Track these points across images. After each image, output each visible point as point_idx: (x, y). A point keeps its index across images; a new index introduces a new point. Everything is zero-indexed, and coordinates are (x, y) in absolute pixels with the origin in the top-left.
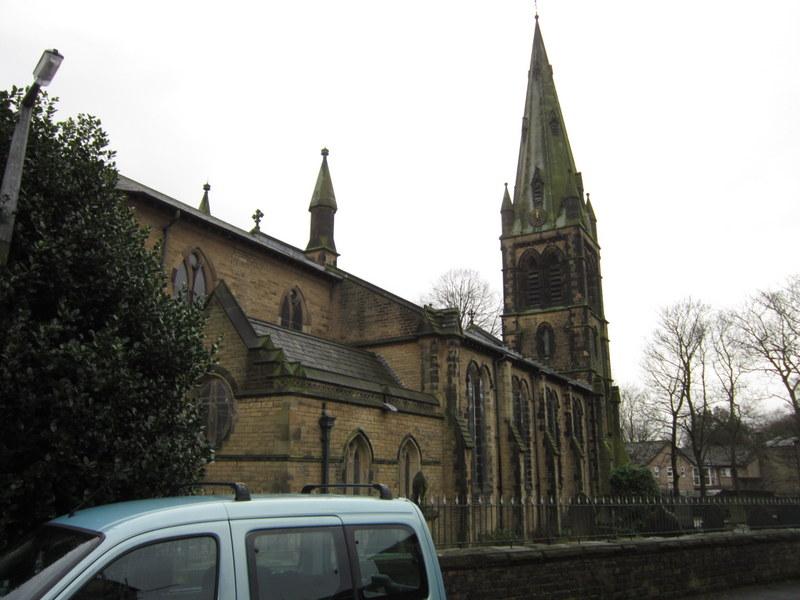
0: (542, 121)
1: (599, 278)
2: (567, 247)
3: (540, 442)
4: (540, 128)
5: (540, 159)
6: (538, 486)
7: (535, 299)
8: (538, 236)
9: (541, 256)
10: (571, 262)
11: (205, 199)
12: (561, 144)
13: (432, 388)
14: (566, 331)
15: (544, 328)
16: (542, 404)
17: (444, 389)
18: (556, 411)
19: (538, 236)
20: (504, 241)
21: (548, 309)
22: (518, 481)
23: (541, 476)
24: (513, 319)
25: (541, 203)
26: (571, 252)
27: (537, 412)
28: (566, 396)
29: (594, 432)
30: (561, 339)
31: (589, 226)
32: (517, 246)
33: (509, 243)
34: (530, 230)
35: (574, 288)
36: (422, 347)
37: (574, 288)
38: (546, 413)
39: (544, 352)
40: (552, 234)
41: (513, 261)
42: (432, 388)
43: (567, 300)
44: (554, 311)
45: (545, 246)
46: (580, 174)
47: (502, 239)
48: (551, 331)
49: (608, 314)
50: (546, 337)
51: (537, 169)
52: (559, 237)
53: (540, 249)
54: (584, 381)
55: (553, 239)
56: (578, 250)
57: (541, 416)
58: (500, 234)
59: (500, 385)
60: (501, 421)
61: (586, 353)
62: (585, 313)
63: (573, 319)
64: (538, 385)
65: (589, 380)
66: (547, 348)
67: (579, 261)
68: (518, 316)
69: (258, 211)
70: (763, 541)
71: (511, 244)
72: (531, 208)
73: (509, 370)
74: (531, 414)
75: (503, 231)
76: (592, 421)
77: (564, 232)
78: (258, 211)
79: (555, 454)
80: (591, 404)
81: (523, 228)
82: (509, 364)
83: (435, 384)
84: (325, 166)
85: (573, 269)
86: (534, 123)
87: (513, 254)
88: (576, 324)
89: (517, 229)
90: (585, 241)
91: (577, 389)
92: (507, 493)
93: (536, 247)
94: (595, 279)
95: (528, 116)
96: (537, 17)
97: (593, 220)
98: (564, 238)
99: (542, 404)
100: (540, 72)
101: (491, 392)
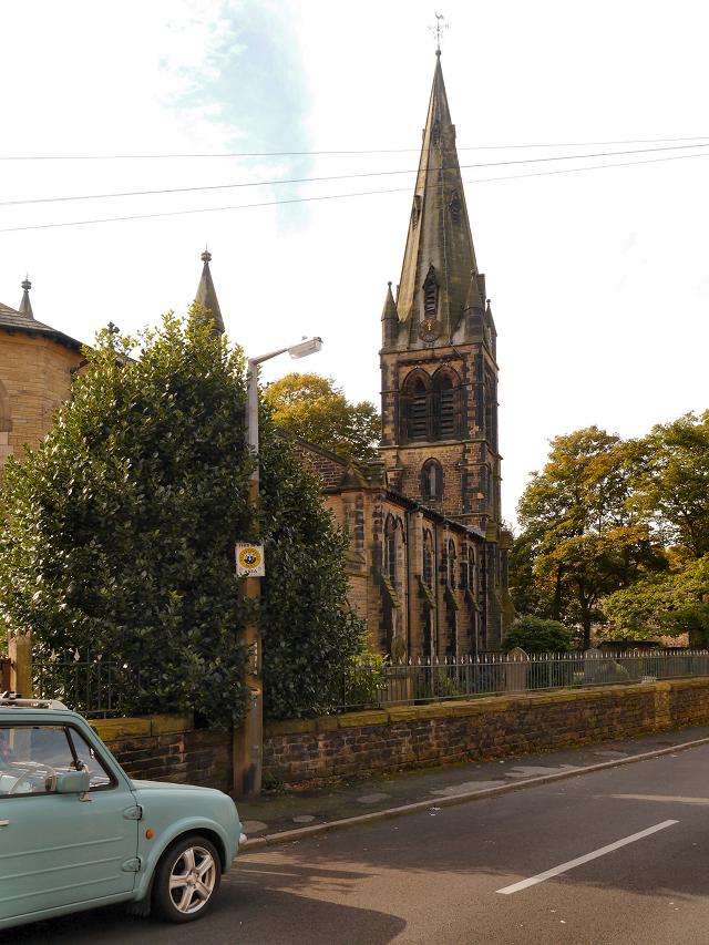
0: (440, 204)
1: (496, 405)
2: (465, 369)
3: (441, 596)
4: (437, 212)
5: (436, 253)
6: (437, 642)
7: (421, 430)
8: (429, 352)
9: (431, 378)
10: (469, 388)
11: (26, 301)
12: (462, 236)
13: (358, 546)
14: (457, 468)
15: (429, 465)
16: (444, 556)
17: (369, 547)
18: (452, 562)
19: (429, 352)
20: (385, 357)
21: (435, 444)
22: (428, 638)
23: (440, 633)
24: (394, 453)
25: (434, 312)
26: (470, 375)
27: (439, 564)
28: (463, 545)
29: (484, 583)
30: (452, 481)
31: (490, 345)
32: (401, 364)
33: (392, 360)
34: (419, 344)
35: (471, 419)
36: (345, 501)
37: (471, 419)
38: (448, 565)
39: (429, 493)
40: (447, 351)
41: (396, 383)
42: (358, 546)
43: (461, 434)
44: (445, 445)
45: (437, 365)
46: (483, 276)
47: (382, 354)
48: (439, 468)
49: (501, 451)
50: (433, 476)
51: (432, 267)
52: (455, 357)
53: (431, 369)
54: (476, 526)
55: (446, 358)
56: (478, 373)
57: (443, 569)
58: (380, 347)
59: (411, 537)
60: (412, 576)
61: (480, 496)
62: (482, 449)
63: (466, 455)
64: (441, 535)
65: (483, 527)
66: (433, 488)
67: (478, 389)
68: (400, 449)
69: (111, 325)
70: (698, 688)
71: (394, 361)
72: (422, 317)
73: (421, 523)
74: (433, 567)
75: (385, 344)
76: (483, 571)
77: (463, 350)
78: (111, 325)
79: (432, 607)
80: (482, 553)
81: (410, 342)
82: (421, 515)
83: (361, 541)
84: (206, 273)
85: (471, 397)
86: (429, 204)
87: (396, 374)
88: (470, 462)
89: (402, 343)
90: (486, 362)
91: (474, 537)
92: (415, 651)
93: (426, 367)
94: (491, 406)
95: (421, 193)
96: (439, 53)
97: (494, 334)
98: (463, 357)
99: (444, 556)
100: (440, 133)
101: (403, 546)
